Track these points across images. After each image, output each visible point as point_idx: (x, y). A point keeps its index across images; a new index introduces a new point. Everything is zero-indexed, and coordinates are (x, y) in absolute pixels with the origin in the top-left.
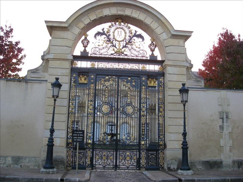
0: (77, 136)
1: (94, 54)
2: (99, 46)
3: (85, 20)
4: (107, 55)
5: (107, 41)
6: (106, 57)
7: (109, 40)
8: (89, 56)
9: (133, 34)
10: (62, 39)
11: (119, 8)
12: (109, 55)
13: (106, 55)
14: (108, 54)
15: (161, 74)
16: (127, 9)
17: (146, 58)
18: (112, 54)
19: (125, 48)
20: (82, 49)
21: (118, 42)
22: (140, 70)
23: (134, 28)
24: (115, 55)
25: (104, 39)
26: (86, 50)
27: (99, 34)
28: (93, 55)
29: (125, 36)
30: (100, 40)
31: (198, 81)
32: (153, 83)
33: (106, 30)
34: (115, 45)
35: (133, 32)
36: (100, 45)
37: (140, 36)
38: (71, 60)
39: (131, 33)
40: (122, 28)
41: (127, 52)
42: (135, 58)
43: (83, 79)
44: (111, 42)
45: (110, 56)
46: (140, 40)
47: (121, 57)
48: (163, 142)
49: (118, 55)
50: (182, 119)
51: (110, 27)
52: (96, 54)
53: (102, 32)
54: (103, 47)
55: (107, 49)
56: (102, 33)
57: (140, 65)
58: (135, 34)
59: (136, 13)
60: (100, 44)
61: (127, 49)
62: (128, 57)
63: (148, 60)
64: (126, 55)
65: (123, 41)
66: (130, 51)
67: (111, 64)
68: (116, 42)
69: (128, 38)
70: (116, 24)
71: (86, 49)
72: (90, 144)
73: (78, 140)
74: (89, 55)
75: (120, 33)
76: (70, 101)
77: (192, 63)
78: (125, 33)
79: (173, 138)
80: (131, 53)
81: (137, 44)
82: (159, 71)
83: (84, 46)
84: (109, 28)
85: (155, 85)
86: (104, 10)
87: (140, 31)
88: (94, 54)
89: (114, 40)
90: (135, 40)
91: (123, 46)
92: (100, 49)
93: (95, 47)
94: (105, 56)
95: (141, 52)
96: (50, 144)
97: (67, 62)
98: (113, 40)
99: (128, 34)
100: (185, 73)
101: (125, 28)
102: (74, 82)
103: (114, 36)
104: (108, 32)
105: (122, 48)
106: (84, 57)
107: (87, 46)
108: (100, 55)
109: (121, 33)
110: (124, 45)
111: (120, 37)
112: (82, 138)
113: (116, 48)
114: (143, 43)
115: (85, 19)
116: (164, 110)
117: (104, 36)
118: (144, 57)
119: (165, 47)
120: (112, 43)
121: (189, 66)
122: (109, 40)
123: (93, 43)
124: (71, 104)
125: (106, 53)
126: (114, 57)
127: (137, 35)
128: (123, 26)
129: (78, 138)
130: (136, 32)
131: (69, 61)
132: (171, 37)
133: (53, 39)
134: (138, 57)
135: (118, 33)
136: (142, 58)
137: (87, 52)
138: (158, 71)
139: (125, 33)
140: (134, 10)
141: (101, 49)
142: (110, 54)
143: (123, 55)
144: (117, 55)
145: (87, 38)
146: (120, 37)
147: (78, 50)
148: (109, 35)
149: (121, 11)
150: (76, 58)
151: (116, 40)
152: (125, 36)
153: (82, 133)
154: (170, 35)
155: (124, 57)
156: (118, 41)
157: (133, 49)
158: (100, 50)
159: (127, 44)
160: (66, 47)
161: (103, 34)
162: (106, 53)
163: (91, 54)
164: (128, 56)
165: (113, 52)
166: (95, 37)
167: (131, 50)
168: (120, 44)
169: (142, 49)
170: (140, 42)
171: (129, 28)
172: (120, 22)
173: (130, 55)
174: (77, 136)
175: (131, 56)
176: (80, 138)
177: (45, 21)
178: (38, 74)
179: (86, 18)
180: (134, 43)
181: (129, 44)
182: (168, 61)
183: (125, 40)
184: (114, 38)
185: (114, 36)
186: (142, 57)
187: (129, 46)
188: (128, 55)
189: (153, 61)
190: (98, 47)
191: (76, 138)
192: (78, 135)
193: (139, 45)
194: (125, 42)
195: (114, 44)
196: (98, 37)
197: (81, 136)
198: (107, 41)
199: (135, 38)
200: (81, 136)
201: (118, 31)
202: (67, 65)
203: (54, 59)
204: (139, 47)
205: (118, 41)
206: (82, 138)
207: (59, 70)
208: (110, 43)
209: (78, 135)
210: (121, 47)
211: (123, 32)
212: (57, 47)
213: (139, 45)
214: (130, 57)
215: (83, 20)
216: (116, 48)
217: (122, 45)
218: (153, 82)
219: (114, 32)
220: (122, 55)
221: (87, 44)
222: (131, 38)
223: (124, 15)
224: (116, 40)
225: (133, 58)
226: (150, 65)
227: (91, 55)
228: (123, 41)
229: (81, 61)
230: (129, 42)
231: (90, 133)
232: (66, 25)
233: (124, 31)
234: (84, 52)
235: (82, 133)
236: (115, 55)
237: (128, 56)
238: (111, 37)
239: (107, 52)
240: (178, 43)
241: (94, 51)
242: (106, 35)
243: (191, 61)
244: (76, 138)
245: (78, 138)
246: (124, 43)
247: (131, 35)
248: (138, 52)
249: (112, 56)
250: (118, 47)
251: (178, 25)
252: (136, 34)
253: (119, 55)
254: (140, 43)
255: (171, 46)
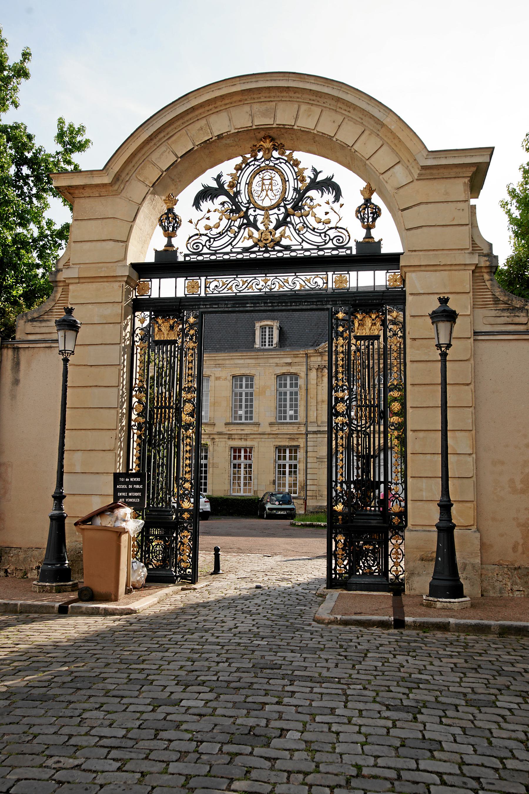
0: (128, 490)
1: (194, 254)
2: (208, 228)
3: (160, 158)
4: (232, 252)
5: (232, 211)
6: (229, 260)
7: (236, 209)
8: (181, 263)
9: (308, 181)
10: (99, 221)
11: (256, 107)
12: (238, 253)
13: (227, 253)
14: (234, 250)
15: (395, 297)
16: (281, 106)
17: (348, 252)
18: (246, 250)
19: (283, 228)
20: (159, 242)
21: (262, 213)
22: (330, 291)
23: (308, 161)
24: (254, 252)
25: (220, 207)
26: (373, 238)
27: (207, 194)
28: (194, 258)
29: (284, 191)
30: (212, 209)
31: (514, 309)
32: (368, 325)
33: (226, 179)
34: (255, 220)
35: (308, 174)
36: (212, 226)
37: (329, 185)
38: (125, 279)
39: (303, 180)
40: (273, 168)
41: (290, 238)
42: (314, 253)
43: (165, 328)
44: (242, 214)
45: (240, 256)
46: (330, 197)
47: (273, 255)
48: (403, 504)
49: (264, 249)
50: (432, 435)
51: (239, 168)
52: (201, 255)
53: (214, 185)
54: (220, 230)
55: (232, 235)
56: (216, 189)
57: (330, 274)
58: (313, 181)
59: (309, 116)
60: (211, 223)
61: (289, 231)
62: (293, 254)
63: (354, 256)
64: (287, 248)
65: (277, 206)
66: (298, 234)
67: (245, 279)
68: (258, 211)
69: (291, 195)
70: (258, 158)
71: (373, 235)
72: (187, 510)
73: (131, 500)
74: (181, 258)
75: (267, 182)
76: (134, 393)
77: (495, 253)
78: (284, 181)
79: (424, 494)
80: (303, 240)
81: (320, 212)
82: (388, 289)
83: (363, 227)
84: (235, 172)
85: (376, 333)
86: (213, 119)
87: (328, 168)
88: (194, 254)
89: (252, 206)
90: (312, 200)
91: (278, 220)
92: (210, 238)
93: (197, 235)
94: (226, 257)
95: (332, 233)
96: (444, 524)
97: (116, 285)
98: (248, 209)
99: (292, 183)
100: (468, 287)
101: (283, 165)
102: (141, 339)
103: (250, 193)
104: (232, 186)
105: (276, 228)
106: (166, 264)
107: (374, 226)
108: (212, 254)
109: (271, 184)
110: (281, 217)
111: (267, 195)
112: (139, 494)
113: (258, 229)
114: (336, 206)
115: (162, 154)
116: (404, 405)
117: (223, 198)
118: (342, 247)
119: (403, 210)
120: (246, 216)
121: (482, 264)
122: (236, 209)
123: (191, 222)
124: (135, 400)
125: (228, 249)
126: (253, 256)
127: (319, 182)
128: (278, 162)
129: (130, 494)
130: (316, 173)
131: (120, 281)
132: (419, 175)
133: (76, 222)
134: (322, 250)
135: (263, 184)
136: (335, 252)
137: (375, 242)
138: (385, 289)
139: (284, 181)
140: (304, 107)
141: (214, 238)
142: (239, 250)
143: (277, 248)
144: (259, 251)
145: (372, 201)
146: (267, 195)
147: (146, 246)
148: (238, 193)
149: (264, 114)
150: (144, 271)
151: (257, 207)
152: (284, 191)
153: (138, 479)
154: (416, 172)
155: (280, 255)
156: (262, 209)
157: (307, 227)
158: (212, 240)
159: (287, 215)
160: (111, 243)
161: (219, 191)
162: (230, 247)
163: (186, 255)
164: (294, 251)
165: (249, 243)
166: (197, 204)
167: (302, 232)
168: (267, 217)
169: (334, 226)
170: (328, 203)
171: (296, 163)
172: (269, 149)
173: (300, 247)
174: (128, 490)
175: (302, 249)
176: (136, 494)
177: (493, 148)
178: (44, 324)
179: (165, 152)
180: (311, 207)
181: (294, 215)
182: (410, 253)
183: (282, 204)
184: (249, 202)
185: (250, 193)
186: (337, 248)
187: (296, 220)
188: (294, 248)
189: (370, 256)
190: (205, 232)
191: (124, 494)
192: (130, 486)
193: (327, 213)
194: (283, 210)
195: (252, 218)
196: (206, 205)
197: (137, 490)
198: (232, 211)
199: (312, 193)
200: (137, 490)
201: (263, 179)
202: (115, 292)
203: (80, 280)
204: (324, 218)
205: (262, 209)
206: (139, 494)
207: (95, 309)
208: (240, 218)
209: (130, 486)
210: (272, 226)
211: (277, 178)
212: (89, 243)
213: (327, 213)
214: (300, 254)
215: (154, 157)
216: (258, 229)
217: (273, 218)
218: (368, 322)
219: (249, 184)
220: (274, 250)
221: (374, 220)
222: (301, 194)
223: (274, 126)
224: (257, 207)
225: (307, 253)
226: (376, 272)
227: (188, 259)
228: (277, 206)
229: (374, 270)
230: (297, 207)
231: (396, 484)
232: (107, 180)
233: (281, 175)
234: (368, 242)
235: (138, 479)
236: (254, 252)
237: (294, 251)
238: (243, 198)
239: (231, 244)
240: (447, 193)
241: (194, 247)
242: (227, 194)
243: (490, 245)
244: (124, 494)
245: (130, 494)
246: (279, 212)
247: (300, 185)
248: (323, 235)
249: (246, 256)
250: (261, 227)
251: (440, 132)
252: (317, 180)
253: (267, 251)
254: (327, 208)
255: (422, 207)
